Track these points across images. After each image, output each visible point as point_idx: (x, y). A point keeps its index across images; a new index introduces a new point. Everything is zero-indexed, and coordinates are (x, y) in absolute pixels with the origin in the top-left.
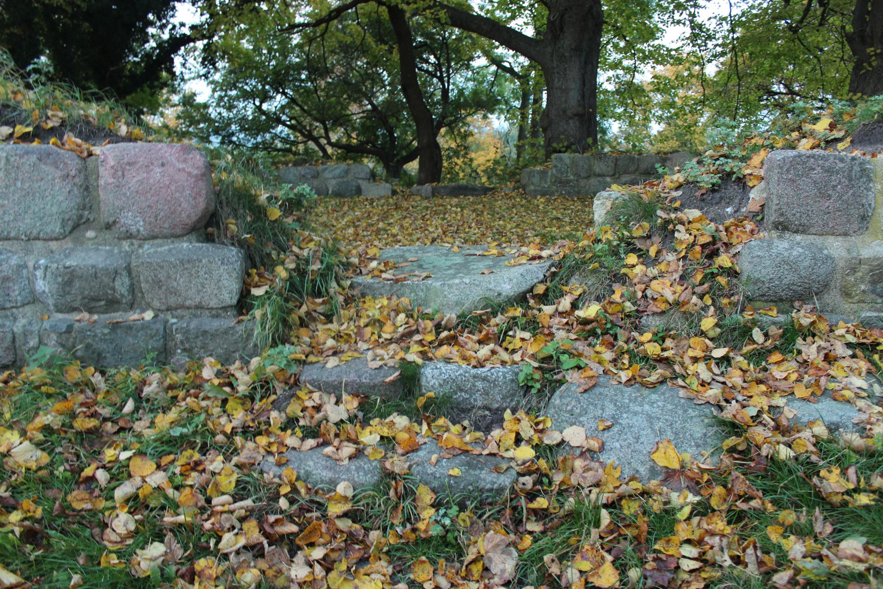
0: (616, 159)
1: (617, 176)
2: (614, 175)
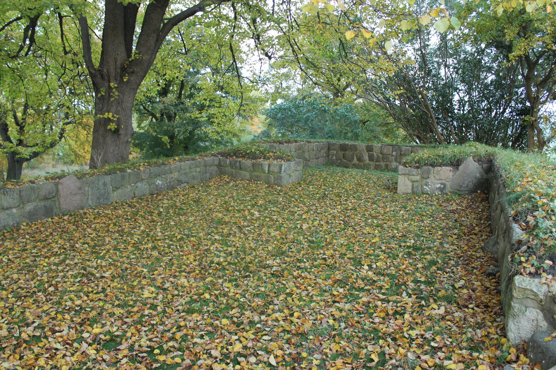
0: (20, 191)
1: (21, 206)
2: (19, 206)
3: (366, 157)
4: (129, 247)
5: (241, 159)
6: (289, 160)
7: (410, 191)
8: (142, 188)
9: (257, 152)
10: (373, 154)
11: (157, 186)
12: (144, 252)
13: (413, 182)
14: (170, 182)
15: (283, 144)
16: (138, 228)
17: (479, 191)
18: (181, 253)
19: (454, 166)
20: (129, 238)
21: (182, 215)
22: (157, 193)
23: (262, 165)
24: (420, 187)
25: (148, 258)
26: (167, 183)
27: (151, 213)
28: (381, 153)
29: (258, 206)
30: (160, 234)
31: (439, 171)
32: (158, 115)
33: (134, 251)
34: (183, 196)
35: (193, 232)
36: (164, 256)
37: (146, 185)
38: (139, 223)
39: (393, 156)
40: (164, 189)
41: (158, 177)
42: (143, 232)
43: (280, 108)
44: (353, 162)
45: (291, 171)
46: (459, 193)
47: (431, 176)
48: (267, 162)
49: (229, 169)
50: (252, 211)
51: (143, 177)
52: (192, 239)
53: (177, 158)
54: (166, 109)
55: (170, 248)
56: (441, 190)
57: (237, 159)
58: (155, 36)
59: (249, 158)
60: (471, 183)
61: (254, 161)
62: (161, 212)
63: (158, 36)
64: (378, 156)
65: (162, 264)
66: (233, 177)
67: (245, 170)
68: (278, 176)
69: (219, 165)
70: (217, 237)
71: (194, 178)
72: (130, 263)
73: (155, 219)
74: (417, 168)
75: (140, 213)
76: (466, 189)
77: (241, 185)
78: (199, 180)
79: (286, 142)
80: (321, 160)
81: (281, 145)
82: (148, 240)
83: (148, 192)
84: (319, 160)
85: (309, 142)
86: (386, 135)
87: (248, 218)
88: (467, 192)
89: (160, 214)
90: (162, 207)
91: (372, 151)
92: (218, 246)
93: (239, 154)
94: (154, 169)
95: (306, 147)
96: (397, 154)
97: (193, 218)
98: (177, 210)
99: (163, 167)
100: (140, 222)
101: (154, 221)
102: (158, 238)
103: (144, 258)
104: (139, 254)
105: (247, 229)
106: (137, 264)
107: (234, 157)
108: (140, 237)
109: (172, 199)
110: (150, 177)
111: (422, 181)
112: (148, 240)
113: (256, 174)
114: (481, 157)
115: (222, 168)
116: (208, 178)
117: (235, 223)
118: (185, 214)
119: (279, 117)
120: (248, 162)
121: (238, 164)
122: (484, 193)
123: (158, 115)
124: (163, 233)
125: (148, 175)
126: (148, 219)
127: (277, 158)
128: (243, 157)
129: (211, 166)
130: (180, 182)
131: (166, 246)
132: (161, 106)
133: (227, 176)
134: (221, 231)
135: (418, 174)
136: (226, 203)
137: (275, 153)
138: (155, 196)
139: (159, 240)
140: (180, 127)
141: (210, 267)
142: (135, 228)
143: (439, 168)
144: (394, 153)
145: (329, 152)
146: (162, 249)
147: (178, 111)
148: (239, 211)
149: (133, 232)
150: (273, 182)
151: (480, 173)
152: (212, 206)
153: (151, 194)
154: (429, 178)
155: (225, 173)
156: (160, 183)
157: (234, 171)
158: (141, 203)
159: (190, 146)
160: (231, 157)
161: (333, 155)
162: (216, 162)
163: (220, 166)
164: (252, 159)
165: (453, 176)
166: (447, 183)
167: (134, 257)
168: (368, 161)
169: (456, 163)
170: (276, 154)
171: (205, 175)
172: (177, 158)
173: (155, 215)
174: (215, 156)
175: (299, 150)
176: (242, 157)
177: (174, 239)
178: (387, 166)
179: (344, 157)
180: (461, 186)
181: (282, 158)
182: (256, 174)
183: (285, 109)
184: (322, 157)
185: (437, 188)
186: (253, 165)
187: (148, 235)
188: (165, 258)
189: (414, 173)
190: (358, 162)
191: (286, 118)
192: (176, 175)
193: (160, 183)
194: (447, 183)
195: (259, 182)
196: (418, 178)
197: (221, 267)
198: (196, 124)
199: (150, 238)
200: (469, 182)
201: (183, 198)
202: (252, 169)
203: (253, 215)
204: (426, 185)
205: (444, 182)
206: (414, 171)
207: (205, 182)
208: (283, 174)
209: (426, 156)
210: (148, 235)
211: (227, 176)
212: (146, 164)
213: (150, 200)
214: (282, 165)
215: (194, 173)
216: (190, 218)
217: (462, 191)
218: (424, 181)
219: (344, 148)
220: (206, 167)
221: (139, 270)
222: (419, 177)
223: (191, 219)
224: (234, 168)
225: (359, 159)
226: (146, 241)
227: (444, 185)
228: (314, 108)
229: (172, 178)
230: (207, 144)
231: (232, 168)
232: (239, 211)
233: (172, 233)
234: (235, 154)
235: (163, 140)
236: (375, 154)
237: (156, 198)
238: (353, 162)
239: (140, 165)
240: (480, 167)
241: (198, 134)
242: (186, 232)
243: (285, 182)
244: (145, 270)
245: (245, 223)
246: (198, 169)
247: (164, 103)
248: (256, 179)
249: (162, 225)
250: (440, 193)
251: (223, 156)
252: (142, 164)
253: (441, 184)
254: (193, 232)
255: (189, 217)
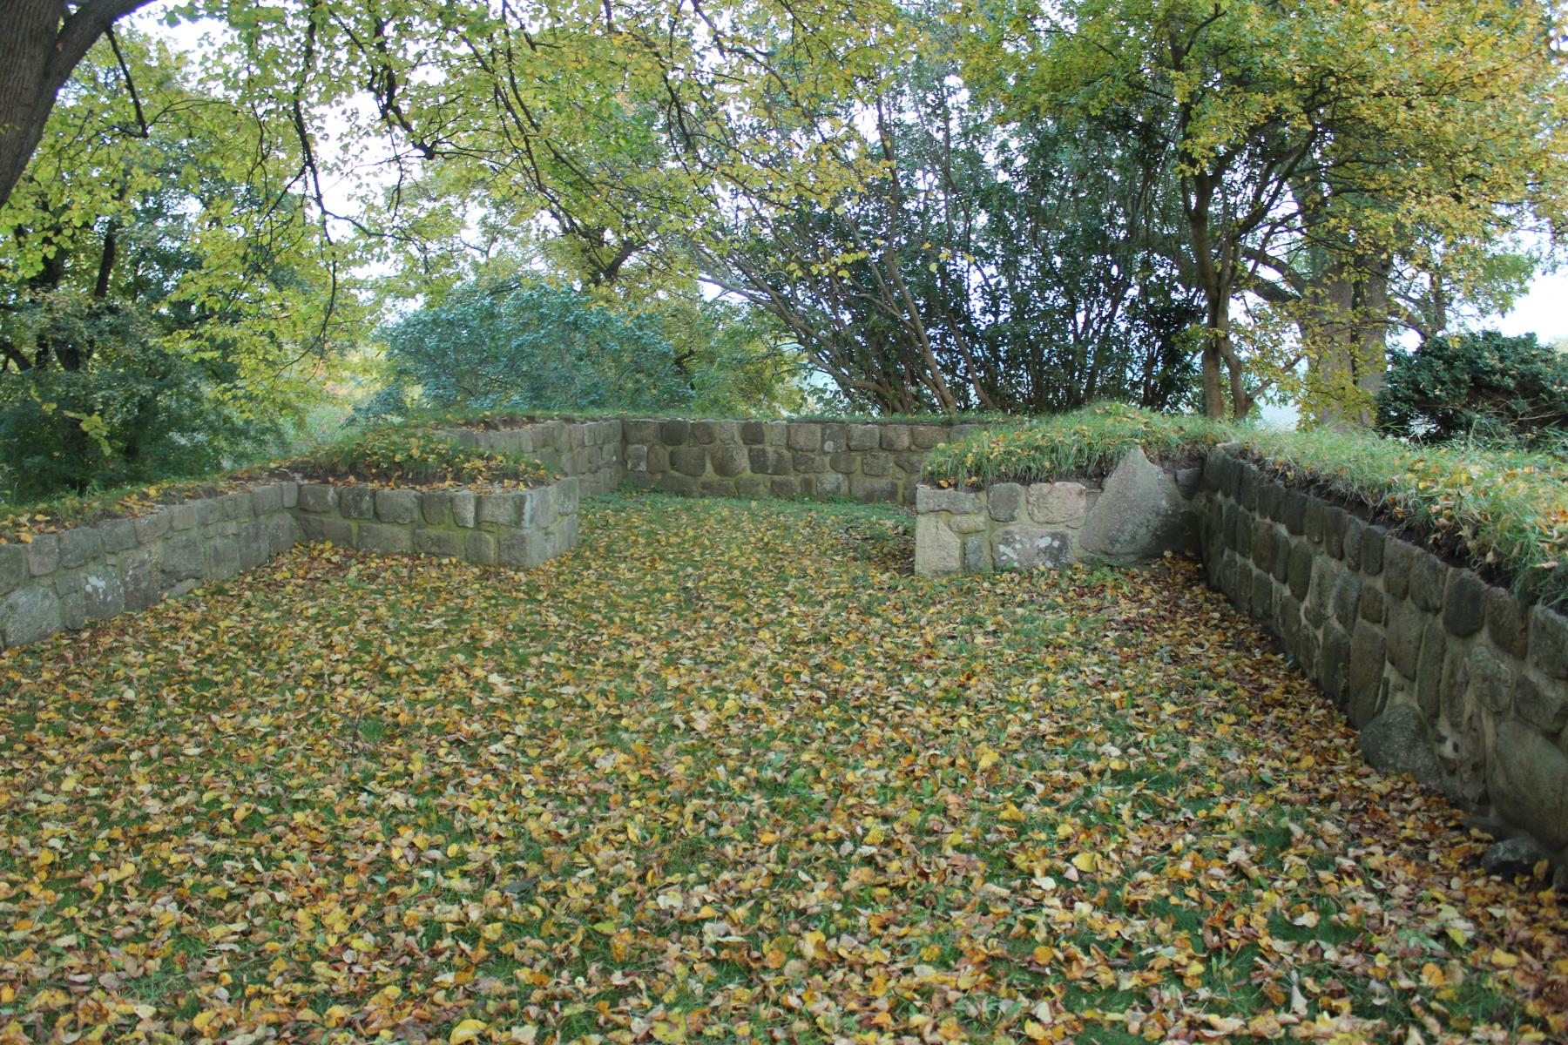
3: (743, 461)
4: (34, 890)
5: (375, 485)
6: (539, 482)
7: (955, 564)
8: (35, 612)
9: (432, 458)
10: (764, 451)
11: (88, 596)
12: (112, 908)
13: (964, 534)
14: (136, 579)
15: (496, 428)
16: (49, 786)
17: (1168, 554)
18: (281, 896)
19: (1090, 478)
20: (23, 841)
21: (216, 710)
22: (92, 625)
23: (452, 500)
24: (986, 551)
25: (138, 937)
26: (125, 583)
27: (90, 712)
28: (789, 447)
29: (486, 651)
30: (153, 806)
31: (1044, 497)
32: (28, 350)
33: (61, 905)
34: (194, 629)
35: (294, 783)
36: (211, 921)
37: (46, 596)
38: (51, 762)
39: (826, 453)
40: (117, 605)
41: (92, 566)
42: (78, 799)
43: (434, 321)
44: (703, 479)
45: (548, 517)
46: (1107, 560)
47: (1022, 515)
48: (468, 492)
49: (335, 520)
50: (478, 672)
51: (35, 570)
52: (299, 817)
53: (152, 492)
54: (59, 329)
55: (219, 872)
56: (1054, 554)
57: (362, 485)
58: (39, 53)
59: (403, 479)
60: (1143, 531)
61: (425, 489)
62: (130, 703)
63: (52, 54)
64: (780, 456)
65: (213, 965)
66: (354, 548)
67: (395, 522)
68: (513, 537)
69: (301, 509)
70: (398, 799)
71: (218, 558)
72: (60, 982)
73: (114, 735)
74: (976, 488)
75: (42, 715)
76: (1128, 550)
77: (387, 575)
78: (237, 564)
79: (505, 423)
80: (605, 475)
81: (492, 433)
82: (112, 841)
83: (57, 623)
84: (600, 475)
85: (569, 420)
86: (747, 396)
87: (476, 701)
88: (1132, 558)
89: (126, 711)
90: (129, 681)
91: (761, 442)
92: (419, 842)
93: (369, 467)
94: (77, 537)
95: (564, 437)
96: (836, 448)
97: (267, 719)
98: (189, 688)
99: (106, 525)
100: (52, 753)
101: (113, 748)
102: (154, 828)
103: (119, 942)
104: (91, 918)
105: (493, 748)
106: (93, 982)
107: (352, 478)
108: (68, 830)
109: (154, 643)
110: (63, 566)
111: (993, 529)
112: (112, 841)
113: (432, 531)
114: (1167, 445)
115: (312, 517)
116: (265, 554)
117: (436, 728)
118: (226, 704)
119: (419, 349)
120: (404, 495)
121: (366, 502)
122: (1186, 558)
123: (28, 350)
124: (165, 801)
125: (56, 558)
126: (83, 740)
127: (500, 475)
128: (384, 476)
129: (271, 512)
130: (171, 576)
131: (200, 862)
132: (41, 319)
133: (329, 545)
134: (400, 766)
135: (980, 509)
136: (365, 645)
137: (489, 458)
138: (85, 635)
139: (162, 836)
140: (110, 387)
141: (435, 954)
142: (39, 784)
143: (1045, 487)
144: (829, 446)
145: (624, 449)
146: (189, 880)
147: (100, 333)
148: (429, 676)
149: (32, 806)
150: (498, 560)
151: (1170, 496)
152: (318, 662)
153: (68, 630)
154: (1013, 518)
155: (322, 536)
156: (101, 584)
157: (354, 526)
158: (39, 669)
159: (143, 448)
160: (338, 477)
161: (639, 458)
162: (290, 500)
163: (304, 510)
164: (416, 481)
165: (1088, 509)
166: (1069, 532)
167: (70, 940)
168: (748, 473)
169: (1095, 469)
170: (493, 463)
171: (254, 546)
172: (152, 492)
173: (106, 717)
174: (283, 476)
175: (544, 446)
176: (377, 477)
177: (225, 826)
178: (807, 485)
179: (672, 464)
180: (1113, 541)
181: (516, 476)
182: (432, 531)
183: (450, 323)
184: (608, 465)
185: (1040, 551)
186: (422, 502)
187: (103, 815)
188: (217, 931)
189: (968, 506)
190: (717, 478)
191: (461, 348)
192: (154, 553)
193: (101, 584)
194: (1069, 532)
195: (445, 561)
196: (980, 520)
197: (483, 952)
198: (162, 370)
199: (117, 833)
200: (1138, 527)
201: (197, 637)
202: (417, 515)
203: (488, 689)
204: (1007, 543)
205: (1060, 529)
206: (967, 500)
207: (258, 569)
208: (528, 529)
209: (999, 450)
210: (103, 815)
211: (329, 545)
212: (39, 517)
213: (70, 655)
214: (522, 499)
215: (218, 542)
216: (254, 722)
217: (1116, 555)
218: (1000, 531)
219: (671, 434)
220: (256, 515)
221: (113, 1018)
222: (981, 519)
223: (261, 723)
224: (354, 514)
225: (722, 468)
226: (101, 846)
227: (1063, 538)
228: (542, 317)
229: (143, 563)
230: (200, 437)
231: (347, 516)
232: (429, 676)
233: (207, 797)
234: (353, 469)
235: (84, 427)
236: (770, 450)
237: (93, 641)
238: (703, 479)
239: (17, 525)
240: (1169, 477)
241: (167, 409)
242: (263, 785)
243: (534, 555)
244: (145, 1011)
245: (476, 727)
246: (232, 527)
247: (50, 310)
248: (434, 549)
249: (148, 761)
250: (1049, 564)
251: (310, 477)
252: (23, 520)
253: (1054, 536)
254: (294, 783)
255: (247, 717)
